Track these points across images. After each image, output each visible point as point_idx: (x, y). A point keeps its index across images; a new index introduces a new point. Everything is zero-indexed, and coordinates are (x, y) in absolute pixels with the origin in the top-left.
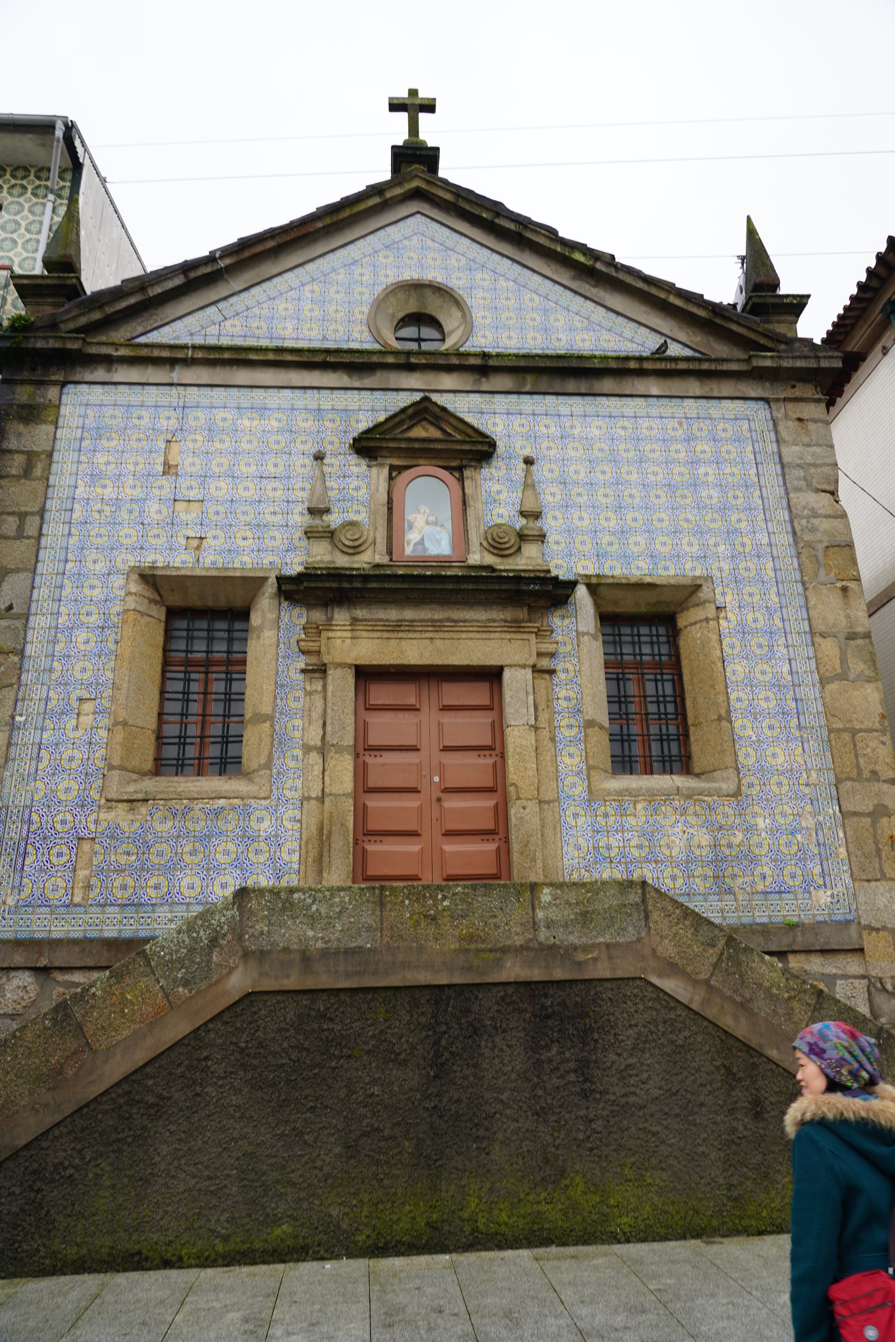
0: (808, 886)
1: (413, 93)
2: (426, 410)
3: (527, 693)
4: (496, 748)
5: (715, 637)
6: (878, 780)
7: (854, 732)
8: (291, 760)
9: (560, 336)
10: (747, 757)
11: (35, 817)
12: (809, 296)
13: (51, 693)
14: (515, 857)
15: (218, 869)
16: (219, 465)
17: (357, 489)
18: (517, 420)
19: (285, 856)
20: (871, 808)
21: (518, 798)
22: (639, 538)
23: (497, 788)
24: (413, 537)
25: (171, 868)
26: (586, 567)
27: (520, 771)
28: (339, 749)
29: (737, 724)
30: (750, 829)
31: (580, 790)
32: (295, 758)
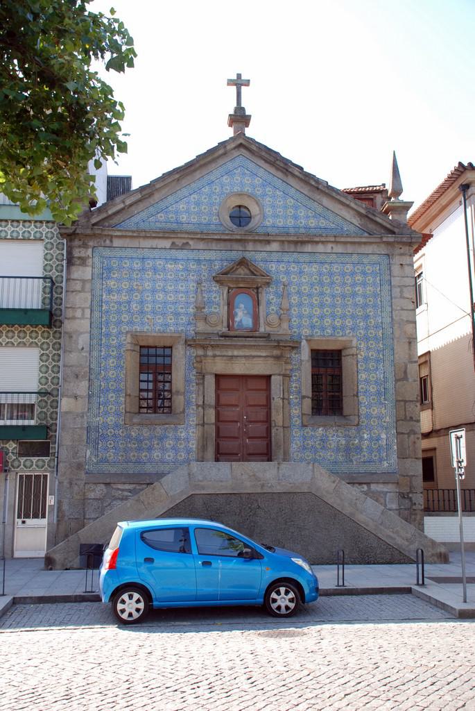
0: (381, 460)
1: (239, 76)
2: (244, 262)
3: (280, 386)
4: (268, 406)
5: (355, 363)
6: (413, 421)
7: (405, 401)
8: (192, 410)
9: (302, 221)
10: (363, 410)
11: (100, 430)
12: (413, 202)
13: (102, 383)
14: (273, 447)
15: (167, 450)
16: (159, 286)
17: (215, 298)
18: (282, 265)
19: (190, 446)
20: (408, 431)
21: (275, 426)
22: (328, 320)
23: (268, 420)
24: (237, 319)
25: (150, 449)
26: (306, 332)
27: (277, 418)
28: (210, 406)
29: (360, 398)
30: (361, 438)
31: (299, 422)
32: (193, 409)
